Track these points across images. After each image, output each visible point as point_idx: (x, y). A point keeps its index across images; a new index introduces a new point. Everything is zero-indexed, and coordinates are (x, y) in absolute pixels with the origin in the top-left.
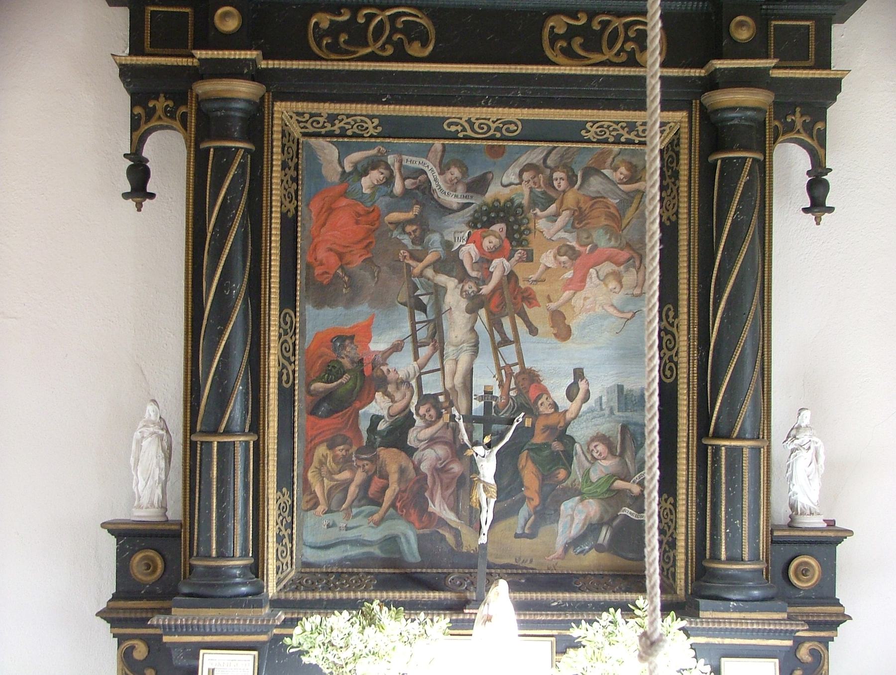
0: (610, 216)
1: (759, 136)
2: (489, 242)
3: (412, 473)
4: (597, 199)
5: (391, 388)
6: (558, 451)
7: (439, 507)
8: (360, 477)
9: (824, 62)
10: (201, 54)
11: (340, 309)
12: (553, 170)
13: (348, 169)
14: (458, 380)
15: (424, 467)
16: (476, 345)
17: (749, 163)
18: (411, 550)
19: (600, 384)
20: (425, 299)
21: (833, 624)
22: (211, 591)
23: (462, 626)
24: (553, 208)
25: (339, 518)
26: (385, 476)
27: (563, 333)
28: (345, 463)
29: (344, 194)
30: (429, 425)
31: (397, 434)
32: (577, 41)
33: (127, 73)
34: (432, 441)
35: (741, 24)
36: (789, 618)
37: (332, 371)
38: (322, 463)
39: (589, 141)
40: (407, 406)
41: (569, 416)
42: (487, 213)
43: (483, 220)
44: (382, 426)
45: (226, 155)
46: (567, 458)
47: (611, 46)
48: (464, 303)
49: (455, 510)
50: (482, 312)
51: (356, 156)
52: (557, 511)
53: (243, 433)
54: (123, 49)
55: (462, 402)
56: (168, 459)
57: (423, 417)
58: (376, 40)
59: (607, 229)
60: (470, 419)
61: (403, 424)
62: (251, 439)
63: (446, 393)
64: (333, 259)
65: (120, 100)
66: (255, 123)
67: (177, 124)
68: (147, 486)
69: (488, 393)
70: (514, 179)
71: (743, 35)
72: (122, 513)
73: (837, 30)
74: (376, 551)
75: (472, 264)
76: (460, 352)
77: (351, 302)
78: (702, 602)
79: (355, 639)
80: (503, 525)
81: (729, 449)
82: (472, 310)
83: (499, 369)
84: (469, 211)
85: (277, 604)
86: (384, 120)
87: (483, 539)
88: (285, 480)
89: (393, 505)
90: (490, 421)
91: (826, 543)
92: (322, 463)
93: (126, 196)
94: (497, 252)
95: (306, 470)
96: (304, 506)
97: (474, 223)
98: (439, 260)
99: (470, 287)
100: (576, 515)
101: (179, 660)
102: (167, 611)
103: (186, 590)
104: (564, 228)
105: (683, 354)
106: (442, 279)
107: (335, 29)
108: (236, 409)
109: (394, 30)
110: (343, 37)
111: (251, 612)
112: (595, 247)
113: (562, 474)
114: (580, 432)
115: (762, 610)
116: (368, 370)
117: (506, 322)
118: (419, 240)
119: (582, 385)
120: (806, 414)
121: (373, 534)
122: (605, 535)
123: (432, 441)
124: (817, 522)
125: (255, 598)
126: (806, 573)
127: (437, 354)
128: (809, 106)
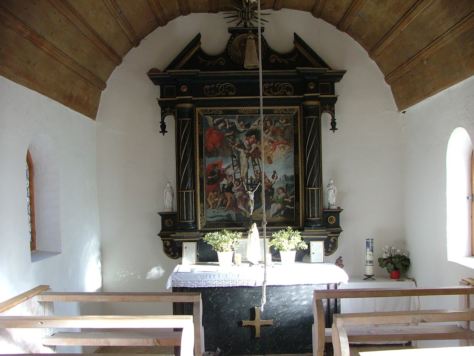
0: (281, 132)
1: (317, 112)
2: (251, 140)
3: (233, 199)
4: (278, 128)
5: (227, 177)
6: (270, 191)
7: (240, 207)
8: (220, 200)
9: (333, 92)
10: (178, 98)
11: (214, 158)
12: (267, 121)
13: (215, 123)
14: (244, 174)
15: (236, 197)
16: (249, 166)
17: (314, 119)
18: (234, 217)
19: (280, 175)
20: (235, 155)
21: (339, 233)
22: (185, 228)
23: (245, 236)
24: (267, 131)
25: (215, 210)
26: (227, 199)
27: (270, 162)
28: (217, 196)
29: (214, 129)
30: (237, 186)
31: (229, 188)
32: (271, 89)
33: (160, 103)
34: (238, 190)
35: (311, 85)
36: (327, 231)
37: (213, 173)
38: (211, 196)
39: (275, 114)
40: (232, 181)
41: (272, 183)
42: (250, 133)
43: (249, 135)
44: (225, 187)
45: (185, 122)
46: (272, 193)
47: (280, 90)
48: (245, 155)
49: (245, 207)
50: (250, 157)
51: (217, 120)
52: (270, 207)
53: (191, 190)
54: (159, 97)
55: (246, 181)
56: (173, 196)
57: (236, 184)
58: (221, 91)
59: (281, 135)
60: (247, 184)
61: (231, 186)
62: (193, 191)
63: (241, 178)
64: (212, 146)
65: (158, 109)
66: (191, 113)
67: (172, 114)
68: (168, 203)
69: (251, 178)
70: (257, 124)
71: (312, 87)
72: (162, 211)
73: (336, 84)
74: (225, 218)
75: (247, 146)
76: (245, 168)
77: (217, 156)
78: (305, 228)
79: (220, 238)
80: (256, 211)
81: (311, 190)
82: (247, 157)
83: (255, 172)
84: (246, 132)
85: (201, 231)
86: (223, 110)
87: (251, 214)
88: (202, 201)
89: (229, 207)
90: (252, 185)
91: (337, 213)
92: (211, 196)
93: (160, 132)
94: (253, 142)
95: (207, 198)
96: (207, 207)
97: (247, 135)
98: (239, 145)
99: (247, 151)
100: (275, 207)
101: (178, 245)
102: (175, 234)
103: (179, 228)
104: (270, 136)
105: (300, 167)
106: (239, 149)
107: (211, 89)
108: (189, 184)
109: (225, 89)
110: (213, 91)
111: (194, 233)
112: (278, 140)
113: (271, 197)
114: (275, 187)
115: (323, 229)
116: (222, 173)
117: (256, 160)
118: (233, 140)
119: (276, 175)
120: (332, 181)
121: (225, 214)
122: (282, 212)
123: (238, 190)
124: (335, 207)
125: (196, 229)
126: (332, 220)
127: (239, 169)
128: (330, 104)
